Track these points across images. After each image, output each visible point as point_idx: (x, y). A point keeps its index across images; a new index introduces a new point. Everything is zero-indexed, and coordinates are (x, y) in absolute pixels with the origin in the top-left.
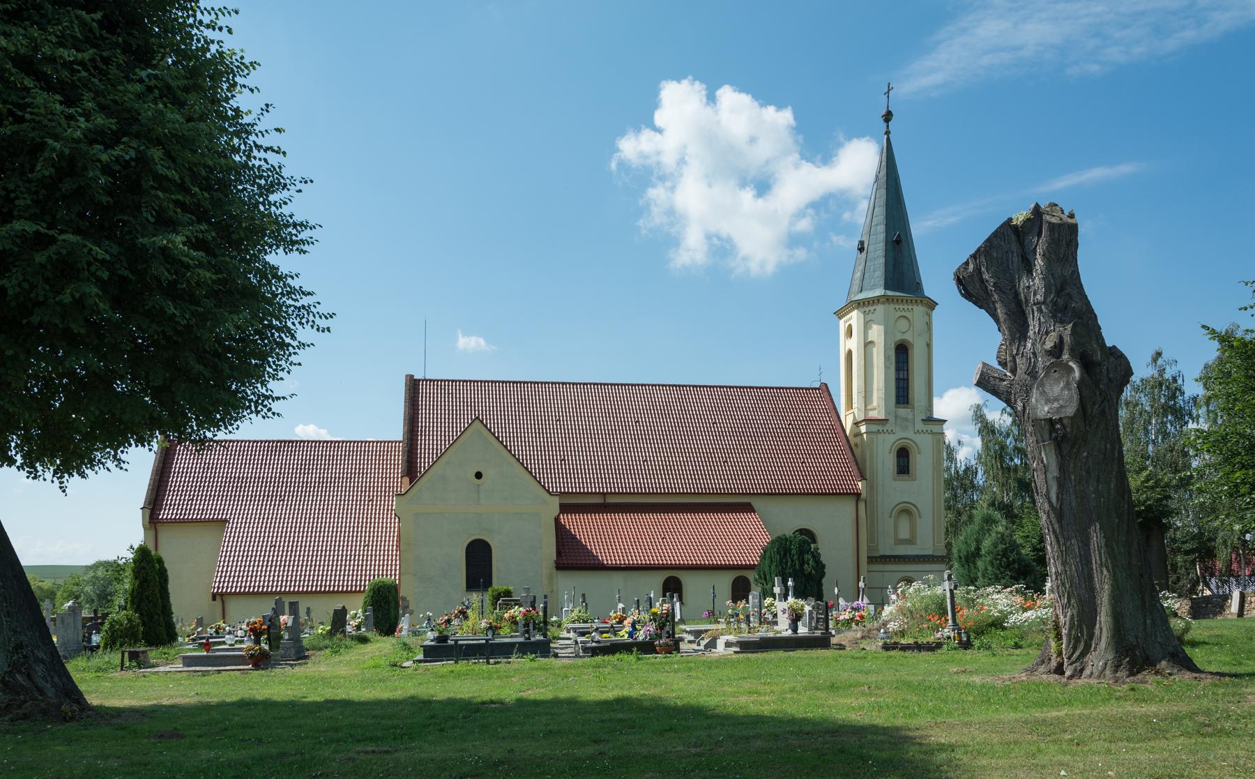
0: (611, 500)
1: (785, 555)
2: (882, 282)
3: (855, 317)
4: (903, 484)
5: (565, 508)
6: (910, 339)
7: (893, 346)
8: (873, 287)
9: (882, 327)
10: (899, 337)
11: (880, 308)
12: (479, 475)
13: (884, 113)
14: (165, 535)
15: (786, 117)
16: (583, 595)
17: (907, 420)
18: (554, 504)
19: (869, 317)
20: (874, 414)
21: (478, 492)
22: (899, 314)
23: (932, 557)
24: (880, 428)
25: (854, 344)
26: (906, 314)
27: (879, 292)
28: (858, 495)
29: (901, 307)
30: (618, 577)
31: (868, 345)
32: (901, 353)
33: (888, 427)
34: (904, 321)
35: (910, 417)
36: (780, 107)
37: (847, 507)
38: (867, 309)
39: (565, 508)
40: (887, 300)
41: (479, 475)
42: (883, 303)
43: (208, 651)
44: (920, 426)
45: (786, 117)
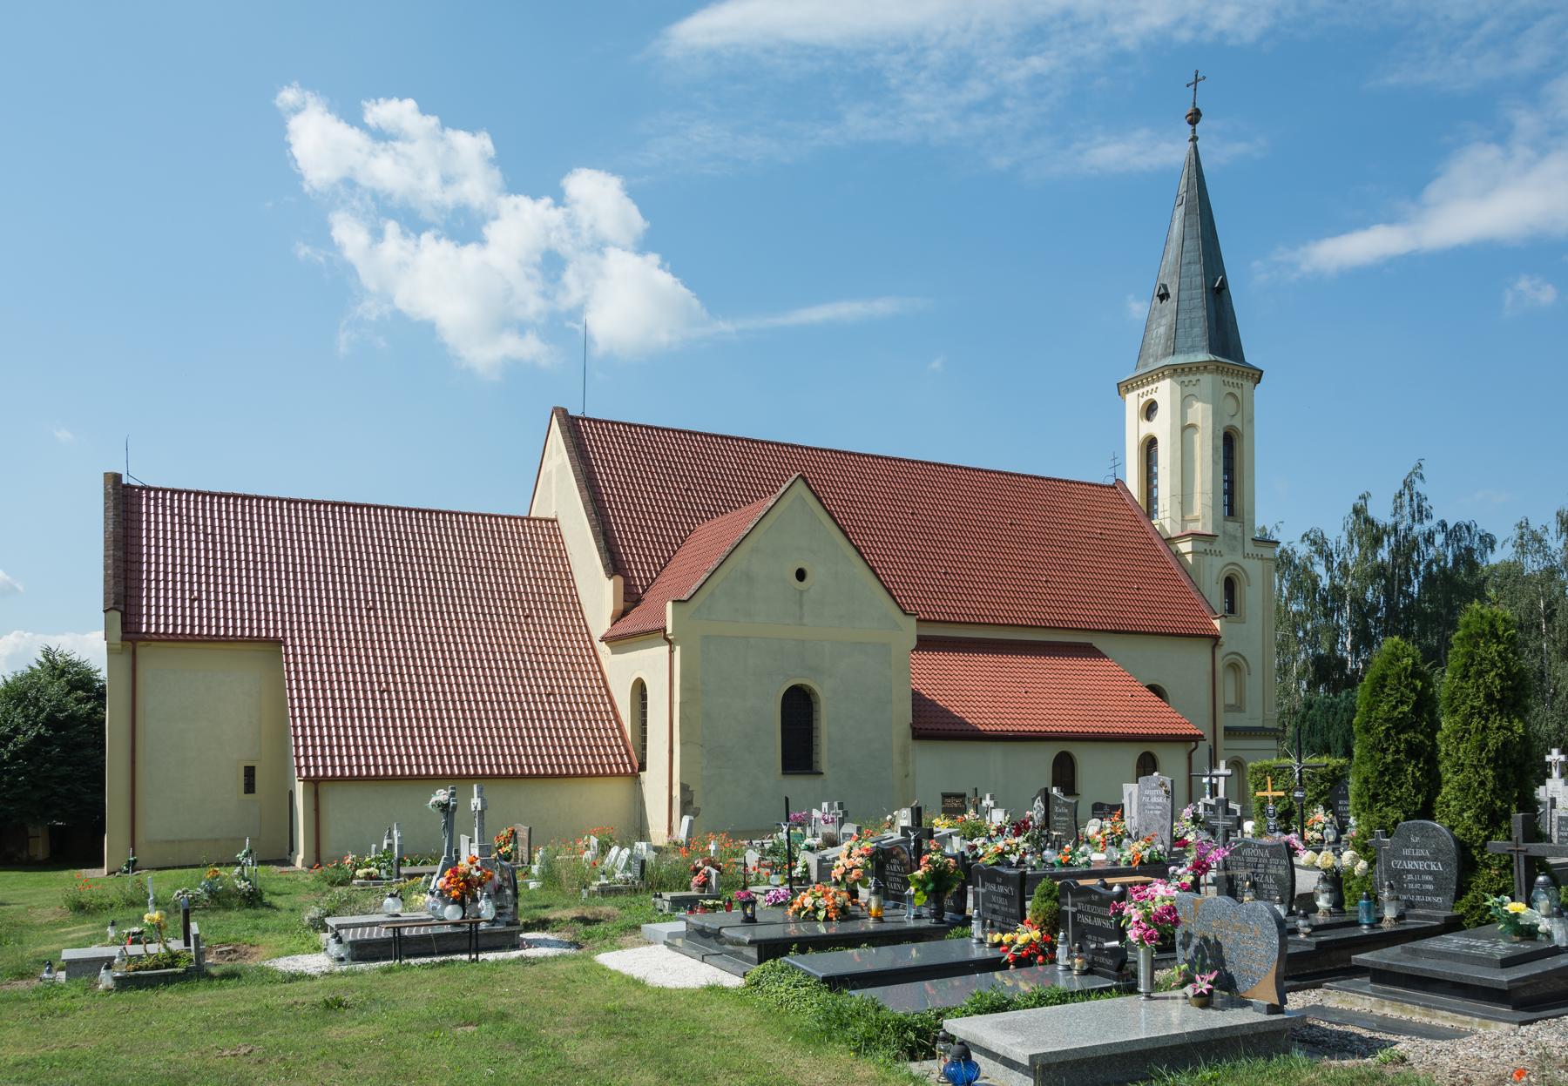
2: (1205, 343)
6: (1239, 426)
8: (1192, 349)
9: (1210, 407)
10: (1227, 422)
11: (1207, 379)
12: (801, 575)
13: (1190, 110)
14: (152, 662)
17: (1235, 538)
19: (1190, 390)
20: (1198, 528)
21: (801, 606)
23: (1262, 729)
24: (1207, 546)
25: (1162, 427)
26: (1237, 392)
27: (1203, 357)
28: (1215, 639)
30: (995, 752)
31: (1187, 429)
32: (1230, 446)
33: (1216, 546)
34: (1231, 402)
37: (1202, 653)
38: (1186, 379)
40: (1218, 369)
41: (801, 575)
44: (1250, 548)
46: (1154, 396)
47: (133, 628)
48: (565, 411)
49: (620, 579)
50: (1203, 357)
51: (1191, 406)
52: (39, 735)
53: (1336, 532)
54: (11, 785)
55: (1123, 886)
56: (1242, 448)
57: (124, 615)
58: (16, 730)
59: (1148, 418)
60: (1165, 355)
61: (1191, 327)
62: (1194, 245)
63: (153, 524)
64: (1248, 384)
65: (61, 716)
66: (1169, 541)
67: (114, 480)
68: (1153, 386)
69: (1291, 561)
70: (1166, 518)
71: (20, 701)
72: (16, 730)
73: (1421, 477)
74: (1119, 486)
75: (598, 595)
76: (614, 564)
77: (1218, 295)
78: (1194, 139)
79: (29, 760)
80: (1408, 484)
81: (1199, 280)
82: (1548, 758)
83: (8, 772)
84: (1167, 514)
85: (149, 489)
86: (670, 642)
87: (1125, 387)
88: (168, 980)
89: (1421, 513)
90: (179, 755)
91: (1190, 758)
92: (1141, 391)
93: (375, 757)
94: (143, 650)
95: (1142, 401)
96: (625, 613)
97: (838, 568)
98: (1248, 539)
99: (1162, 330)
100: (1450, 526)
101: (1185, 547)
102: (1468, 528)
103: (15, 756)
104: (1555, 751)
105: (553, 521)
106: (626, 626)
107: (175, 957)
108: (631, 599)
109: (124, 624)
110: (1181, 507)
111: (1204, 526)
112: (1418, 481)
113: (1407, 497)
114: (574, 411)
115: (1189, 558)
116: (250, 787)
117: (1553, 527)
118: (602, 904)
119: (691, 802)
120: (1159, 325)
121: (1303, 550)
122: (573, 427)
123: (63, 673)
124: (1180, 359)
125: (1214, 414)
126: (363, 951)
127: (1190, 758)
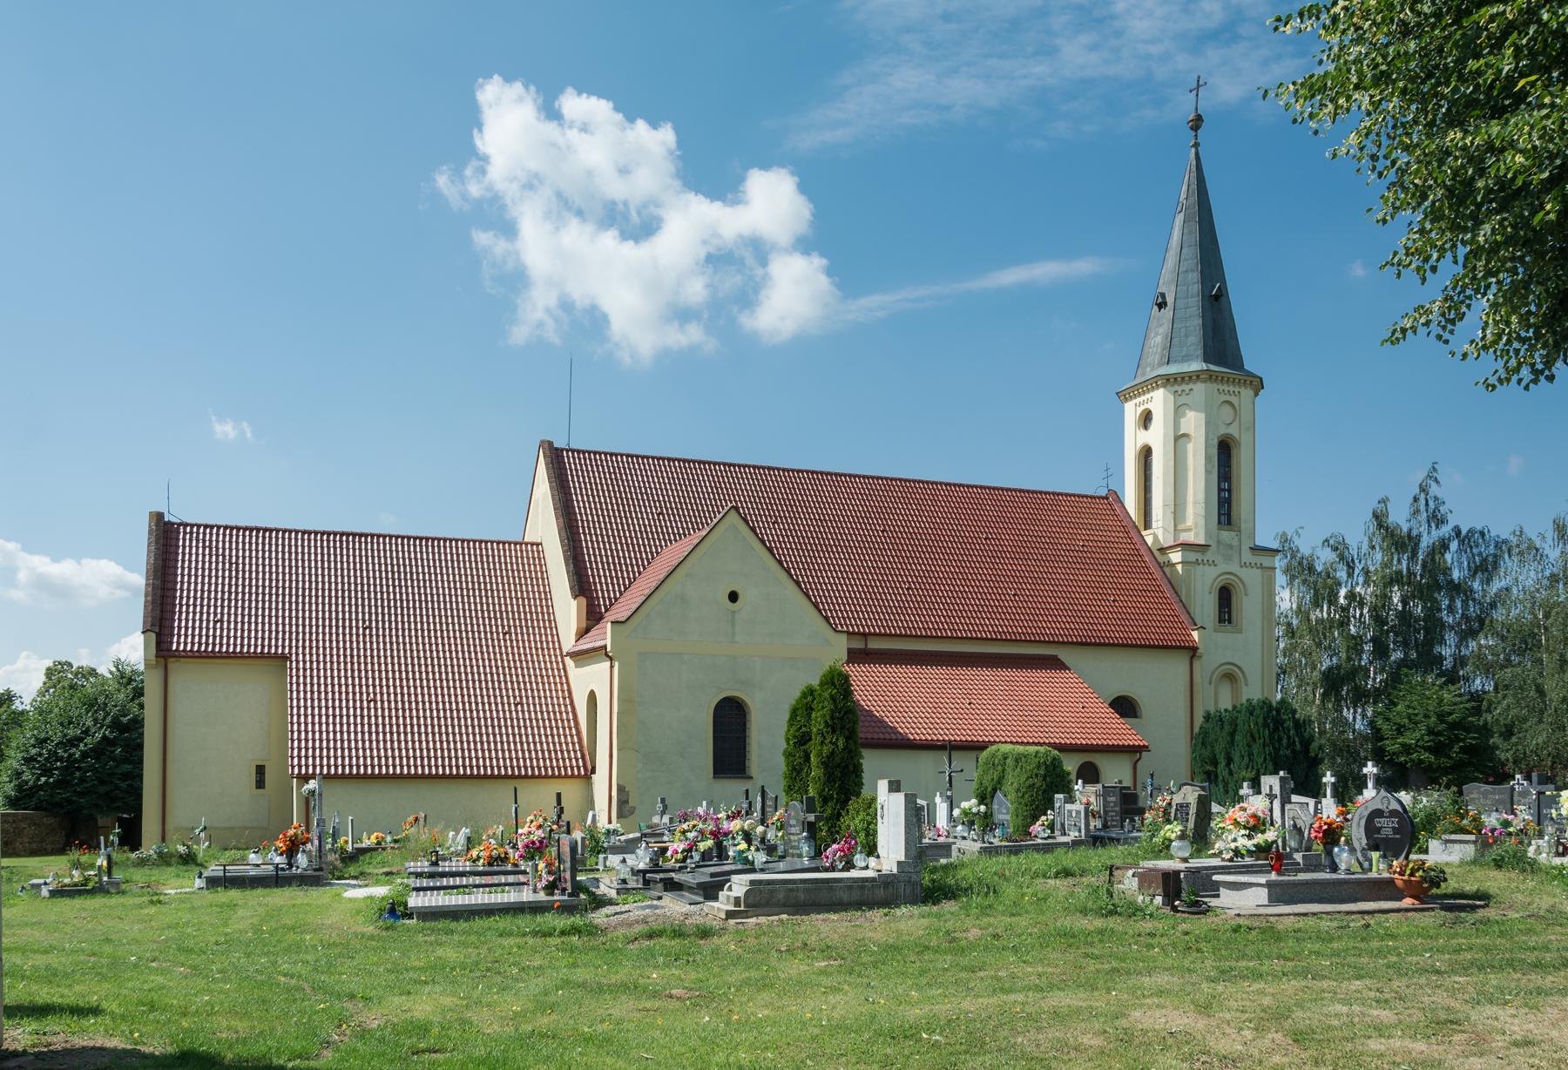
0: (874, 644)
1: (1276, 729)
2: (1200, 352)
3: (1158, 400)
4: (1224, 638)
5: (855, 656)
6: (1236, 435)
7: (1216, 442)
8: (1186, 358)
10: (1223, 430)
11: (1199, 388)
12: (733, 597)
15: (666, 136)
16: (663, 801)
17: (1231, 547)
18: (835, 651)
19: (1182, 400)
21: (733, 625)
22: (1224, 398)
24: (1199, 556)
25: (1156, 437)
26: (1234, 399)
27: (1196, 366)
28: (1193, 651)
29: (1226, 388)
31: (1180, 438)
32: (1225, 453)
33: (1209, 556)
34: (1228, 408)
35: (1235, 543)
36: (654, 124)
38: (1179, 388)
39: (855, 656)
40: (1211, 377)
41: (733, 597)
42: (1205, 381)
43: (1279, 873)
44: (1247, 556)
45: (666, 136)
46: (1149, 406)
47: (165, 646)
48: (550, 443)
49: (583, 601)
50: (1196, 366)
51: (1184, 415)
52: (104, 737)
53: (1357, 535)
54: (82, 780)
55: (850, 866)
56: (1242, 458)
57: (158, 635)
58: (86, 732)
59: (1146, 428)
60: (1160, 365)
61: (1187, 336)
62: (1192, 253)
63: (189, 555)
64: (1247, 393)
65: (125, 720)
66: (1162, 550)
67: (159, 517)
68: (1148, 396)
69: (1311, 569)
70: (1158, 532)
71: (92, 706)
72: (86, 732)
73: (1437, 481)
74: (1112, 499)
75: (567, 611)
76: (581, 585)
77: (1215, 305)
78: (1196, 145)
79: (97, 759)
80: (1423, 489)
81: (1196, 288)
82: (1365, 770)
83: (79, 769)
84: (1160, 524)
85: (186, 525)
86: (611, 659)
87: (1125, 396)
88: (80, 893)
89: (1437, 519)
90: (203, 754)
91: (1135, 768)
92: (1138, 400)
93: (358, 758)
94: (173, 665)
95: (1140, 410)
96: (587, 631)
97: (769, 589)
98: (1245, 548)
99: (1159, 339)
100: (1464, 532)
101: (1175, 557)
102: (1482, 534)
103: (85, 755)
104: (1370, 764)
105: (537, 545)
106: (585, 645)
107: (87, 880)
108: (593, 617)
109: (158, 643)
110: (1174, 516)
111: (1196, 536)
112: (1433, 484)
113: (1423, 502)
114: (559, 443)
115: (1179, 567)
116: (260, 784)
117: (1550, 534)
118: (687, 916)
119: (627, 802)
120: (1157, 334)
121: (1325, 557)
122: (556, 458)
123: (130, 680)
124: (1173, 369)
125: (1207, 423)
126: (213, 882)
127: (1135, 768)
